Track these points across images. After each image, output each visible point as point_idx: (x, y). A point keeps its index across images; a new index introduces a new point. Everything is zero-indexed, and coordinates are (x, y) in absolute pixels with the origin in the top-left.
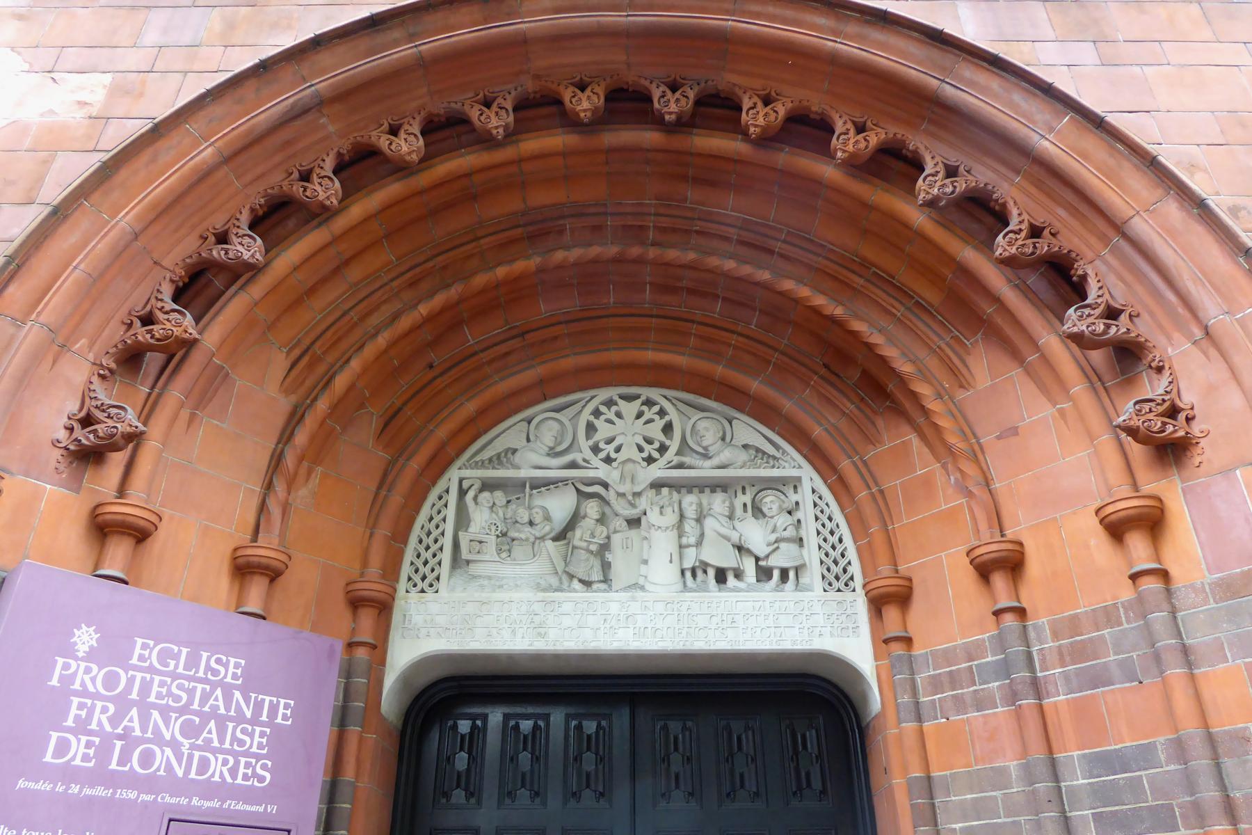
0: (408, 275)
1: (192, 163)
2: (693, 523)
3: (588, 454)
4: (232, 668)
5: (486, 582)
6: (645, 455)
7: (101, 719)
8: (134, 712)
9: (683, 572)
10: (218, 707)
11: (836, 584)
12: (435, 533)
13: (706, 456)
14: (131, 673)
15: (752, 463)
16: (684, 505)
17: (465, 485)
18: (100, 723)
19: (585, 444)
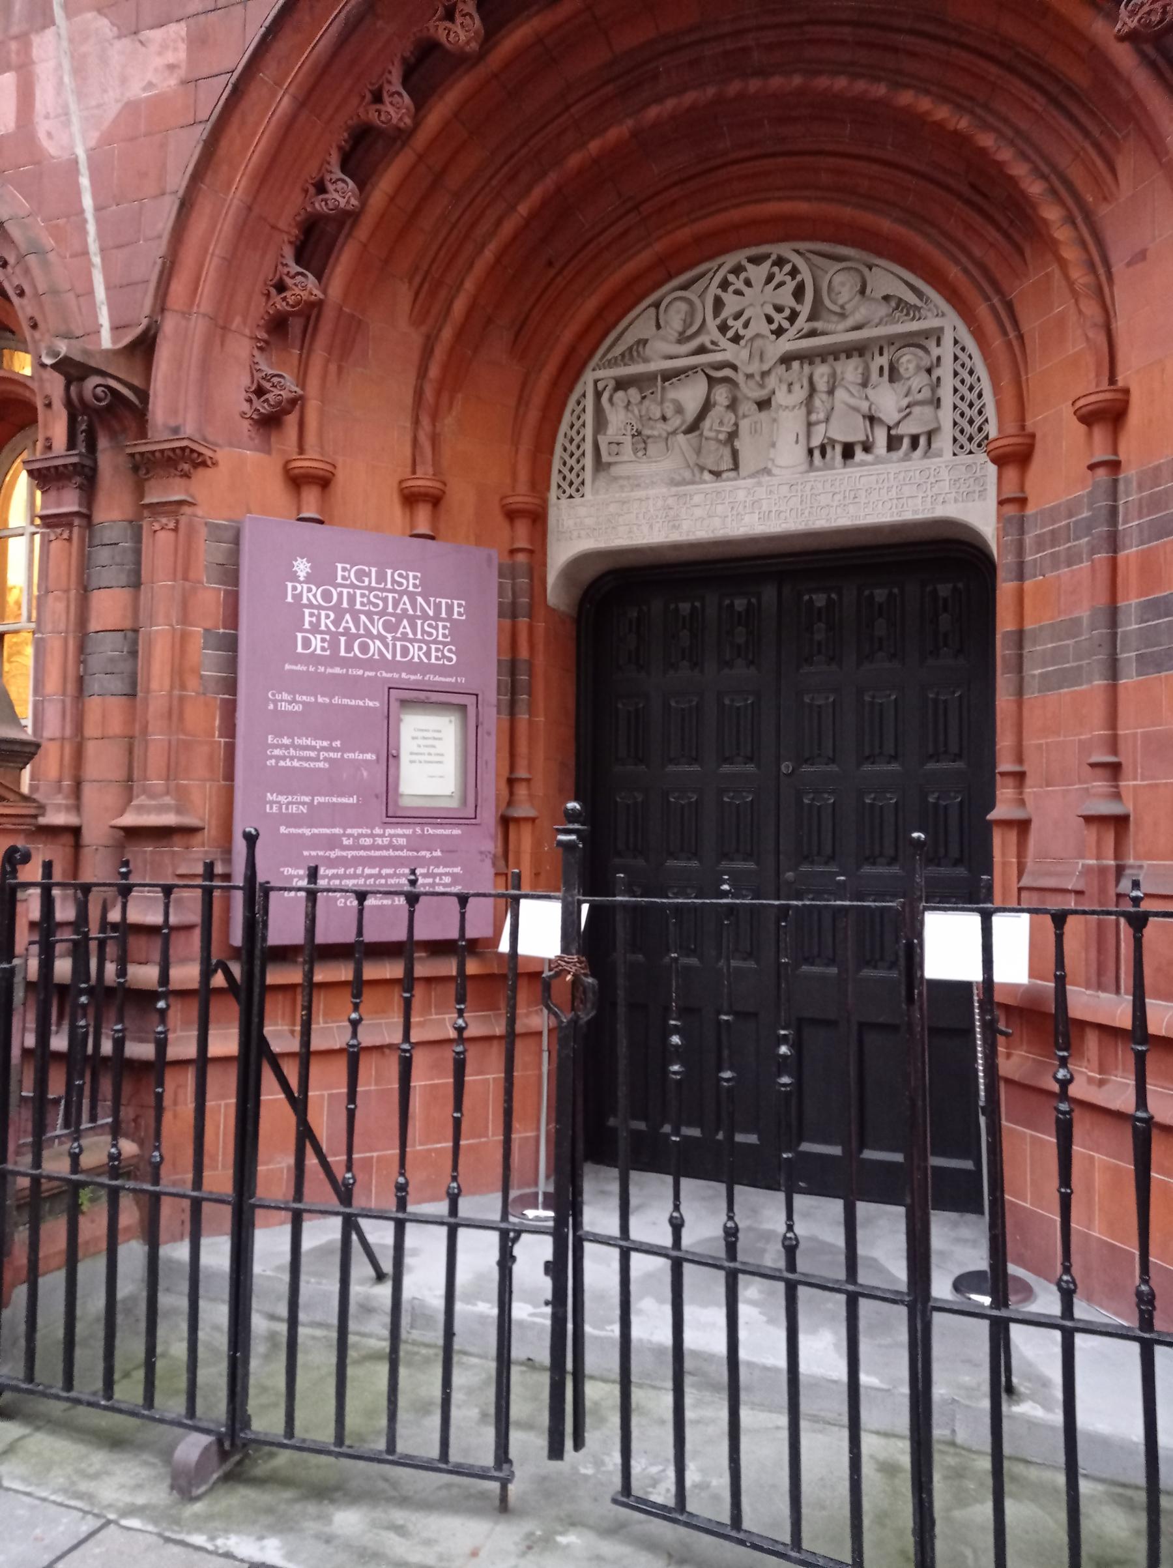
0: (506, 169)
1: (275, 118)
2: (824, 397)
3: (716, 334)
4: (412, 580)
5: (625, 482)
6: (774, 326)
7: (326, 623)
8: (348, 617)
9: (810, 452)
10: (407, 610)
11: (968, 447)
12: (577, 439)
13: (843, 316)
14: (339, 589)
15: (890, 319)
16: (816, 378)
17: (600, 388)
18: (326, 625)
19: (712, 324)
